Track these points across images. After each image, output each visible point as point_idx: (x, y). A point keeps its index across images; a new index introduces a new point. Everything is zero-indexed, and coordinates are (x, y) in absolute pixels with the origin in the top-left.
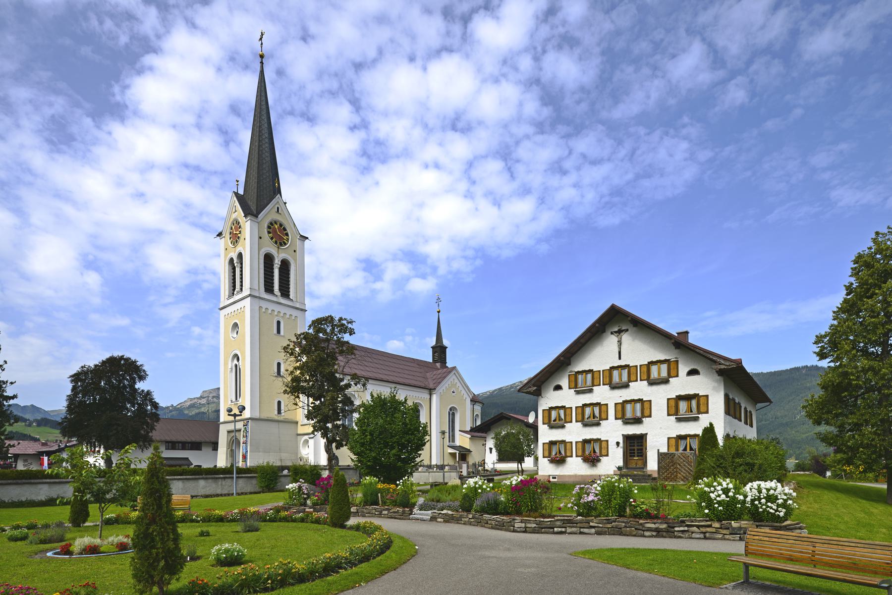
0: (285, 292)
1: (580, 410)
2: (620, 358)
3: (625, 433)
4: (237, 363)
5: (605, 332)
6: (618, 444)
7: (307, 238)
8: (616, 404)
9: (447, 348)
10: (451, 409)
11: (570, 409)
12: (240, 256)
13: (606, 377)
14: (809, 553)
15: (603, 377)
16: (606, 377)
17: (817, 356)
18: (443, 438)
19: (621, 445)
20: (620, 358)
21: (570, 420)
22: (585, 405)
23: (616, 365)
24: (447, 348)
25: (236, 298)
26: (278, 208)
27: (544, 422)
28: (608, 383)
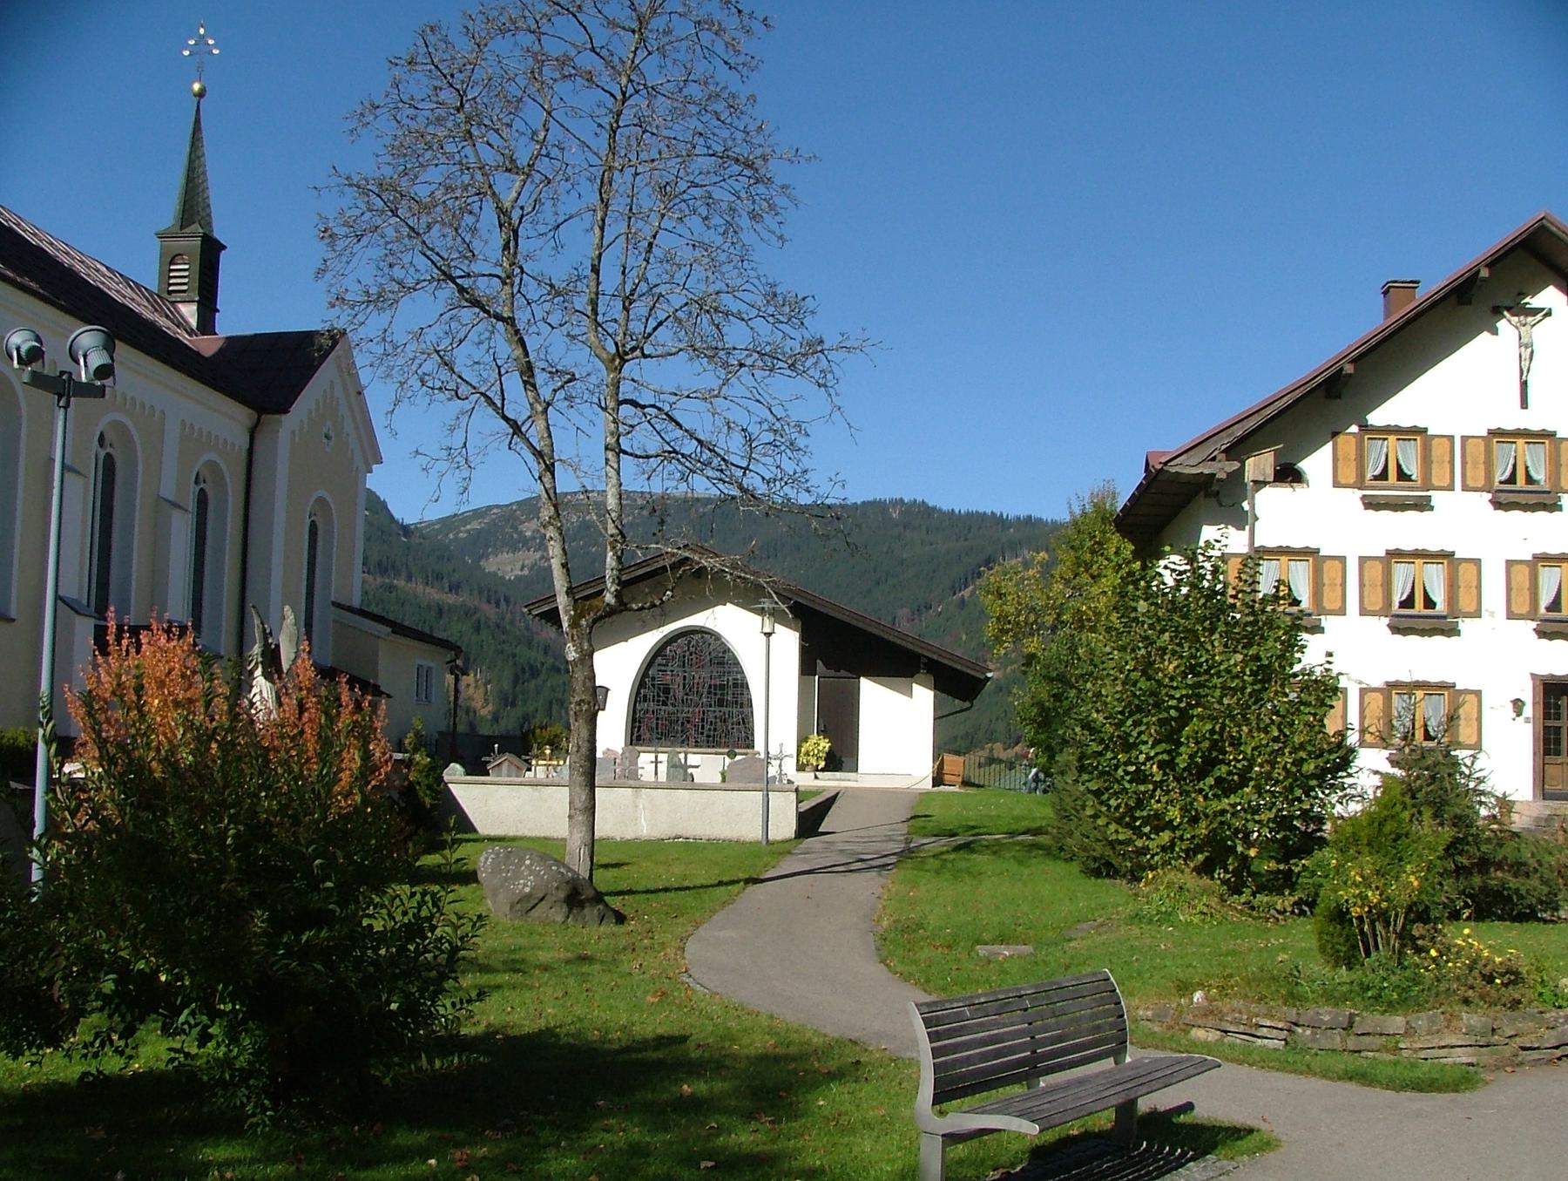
1: (1376, 571)
2: (1524, 404)
3: (1544, 670)
5: (1470, 303)
6: (1518, 705)
8: (1510, 564)
9: (224, 247)
11: (1472, 567)
13: (1475, 463)
14: (1021, 1048)
15: (1464, 463)
16: (1475, 463)
17: (371, 471)
18: (768, 635)
19: (1528, 711)
20: (1524, 404)
21: (1337, 605)
22: (1396, 555)
23: (1509, 426)
24: (224, 247)
27: (1514, 609)
28: (1480, 484)
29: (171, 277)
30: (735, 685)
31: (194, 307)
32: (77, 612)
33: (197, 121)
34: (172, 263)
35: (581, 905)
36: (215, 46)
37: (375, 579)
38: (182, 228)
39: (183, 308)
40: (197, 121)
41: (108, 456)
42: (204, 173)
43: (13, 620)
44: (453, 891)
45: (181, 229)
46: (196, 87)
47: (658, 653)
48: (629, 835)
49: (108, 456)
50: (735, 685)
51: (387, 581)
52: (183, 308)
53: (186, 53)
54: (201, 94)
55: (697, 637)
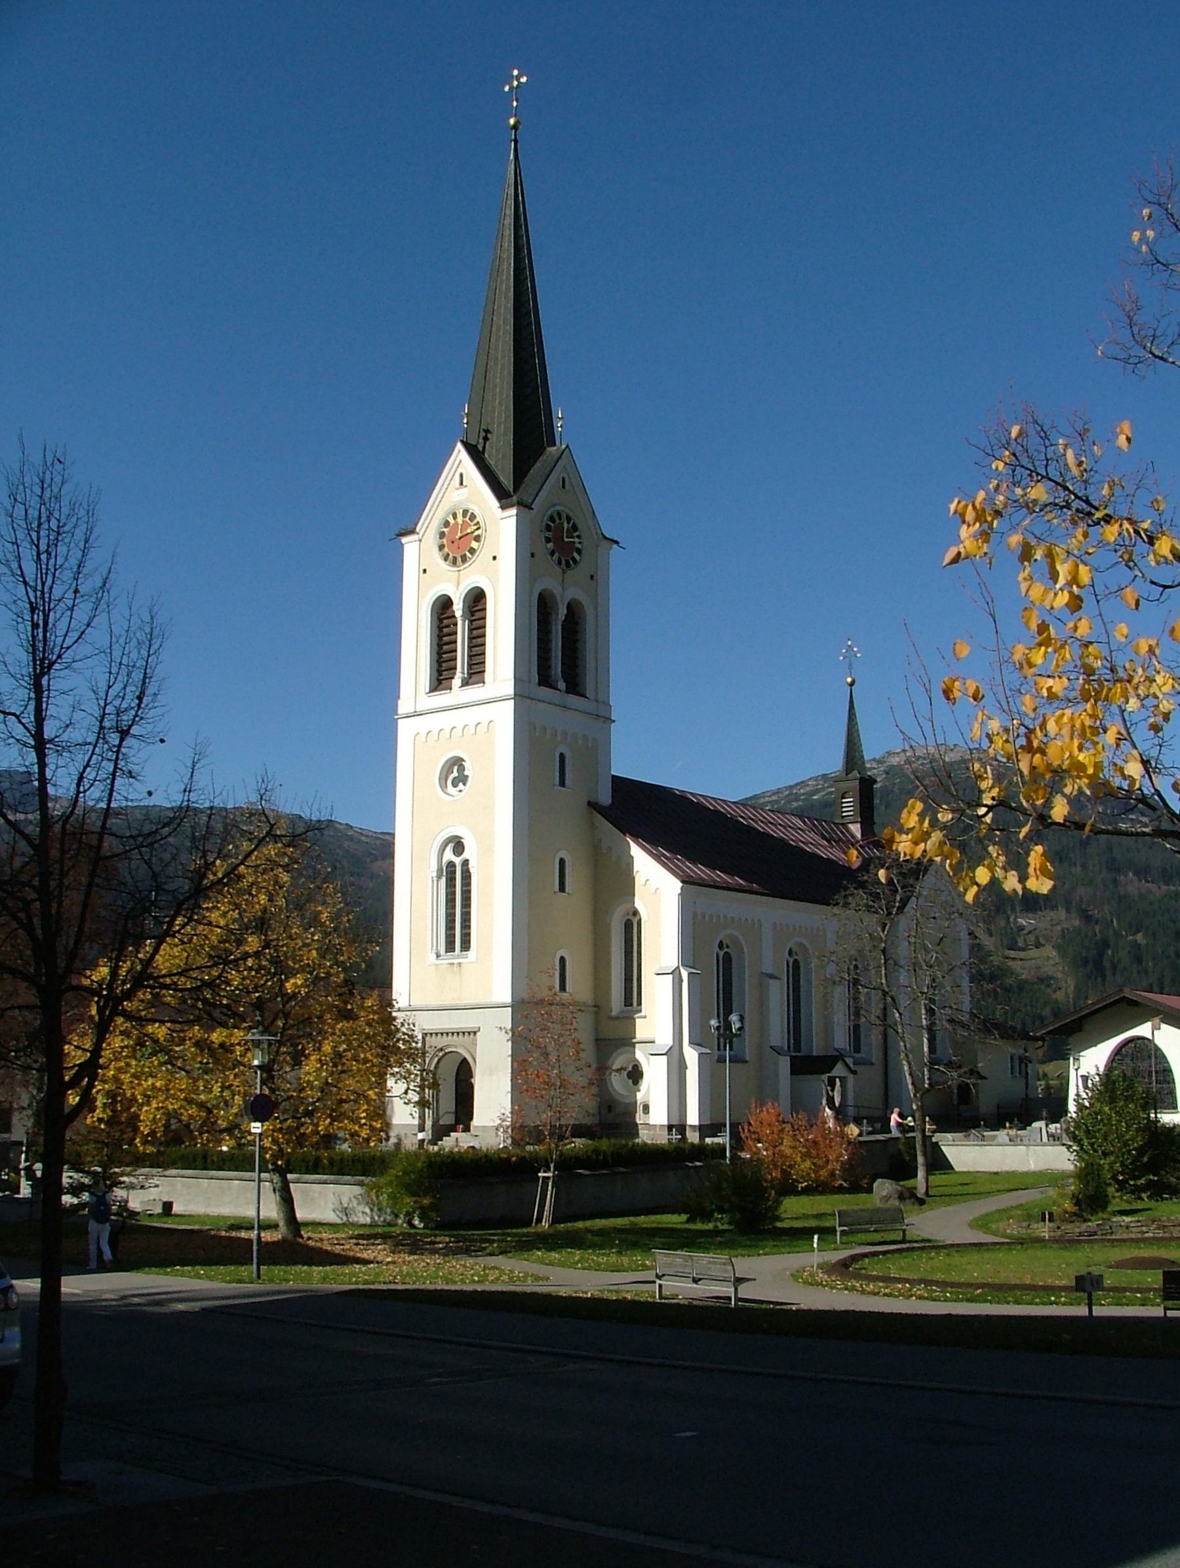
0: (575, 686)
4: (458, 861)
7: (617, 542)
10: (721, 946)
12: (476, 599)
25: (457, 693)
26: (564, 480)
29: (725, 1040)
30: (1164, 1070)
31: (859, 825)
32: (779, 1054)
33: (851, 702)
34: (843, 797)
35: (905, 1199)
36: (858, 652)
37: (1159, 888)
38: (847, 775)
39: (851, 826)
40: (851, 702)
41: (796, 961)
42: (859, 735)
43: (747, 1062)
44: (157, 1186)
45: (847, 775)
46: (849, 680)
47: (1118, 1051)
48: (1025, 1170)
49: (796, 961)
50: (1164, 1070)
51: (1172, 888)
52: (851, 826)
53: (841, 658)
54: (852, 684)
55: (1139, 1042)
